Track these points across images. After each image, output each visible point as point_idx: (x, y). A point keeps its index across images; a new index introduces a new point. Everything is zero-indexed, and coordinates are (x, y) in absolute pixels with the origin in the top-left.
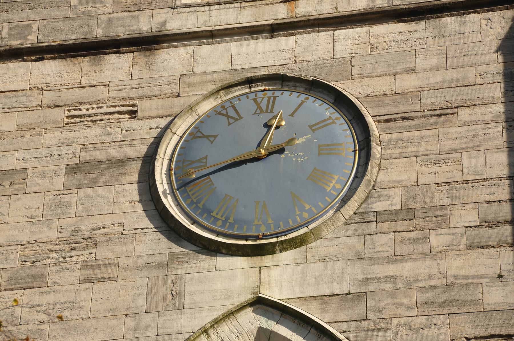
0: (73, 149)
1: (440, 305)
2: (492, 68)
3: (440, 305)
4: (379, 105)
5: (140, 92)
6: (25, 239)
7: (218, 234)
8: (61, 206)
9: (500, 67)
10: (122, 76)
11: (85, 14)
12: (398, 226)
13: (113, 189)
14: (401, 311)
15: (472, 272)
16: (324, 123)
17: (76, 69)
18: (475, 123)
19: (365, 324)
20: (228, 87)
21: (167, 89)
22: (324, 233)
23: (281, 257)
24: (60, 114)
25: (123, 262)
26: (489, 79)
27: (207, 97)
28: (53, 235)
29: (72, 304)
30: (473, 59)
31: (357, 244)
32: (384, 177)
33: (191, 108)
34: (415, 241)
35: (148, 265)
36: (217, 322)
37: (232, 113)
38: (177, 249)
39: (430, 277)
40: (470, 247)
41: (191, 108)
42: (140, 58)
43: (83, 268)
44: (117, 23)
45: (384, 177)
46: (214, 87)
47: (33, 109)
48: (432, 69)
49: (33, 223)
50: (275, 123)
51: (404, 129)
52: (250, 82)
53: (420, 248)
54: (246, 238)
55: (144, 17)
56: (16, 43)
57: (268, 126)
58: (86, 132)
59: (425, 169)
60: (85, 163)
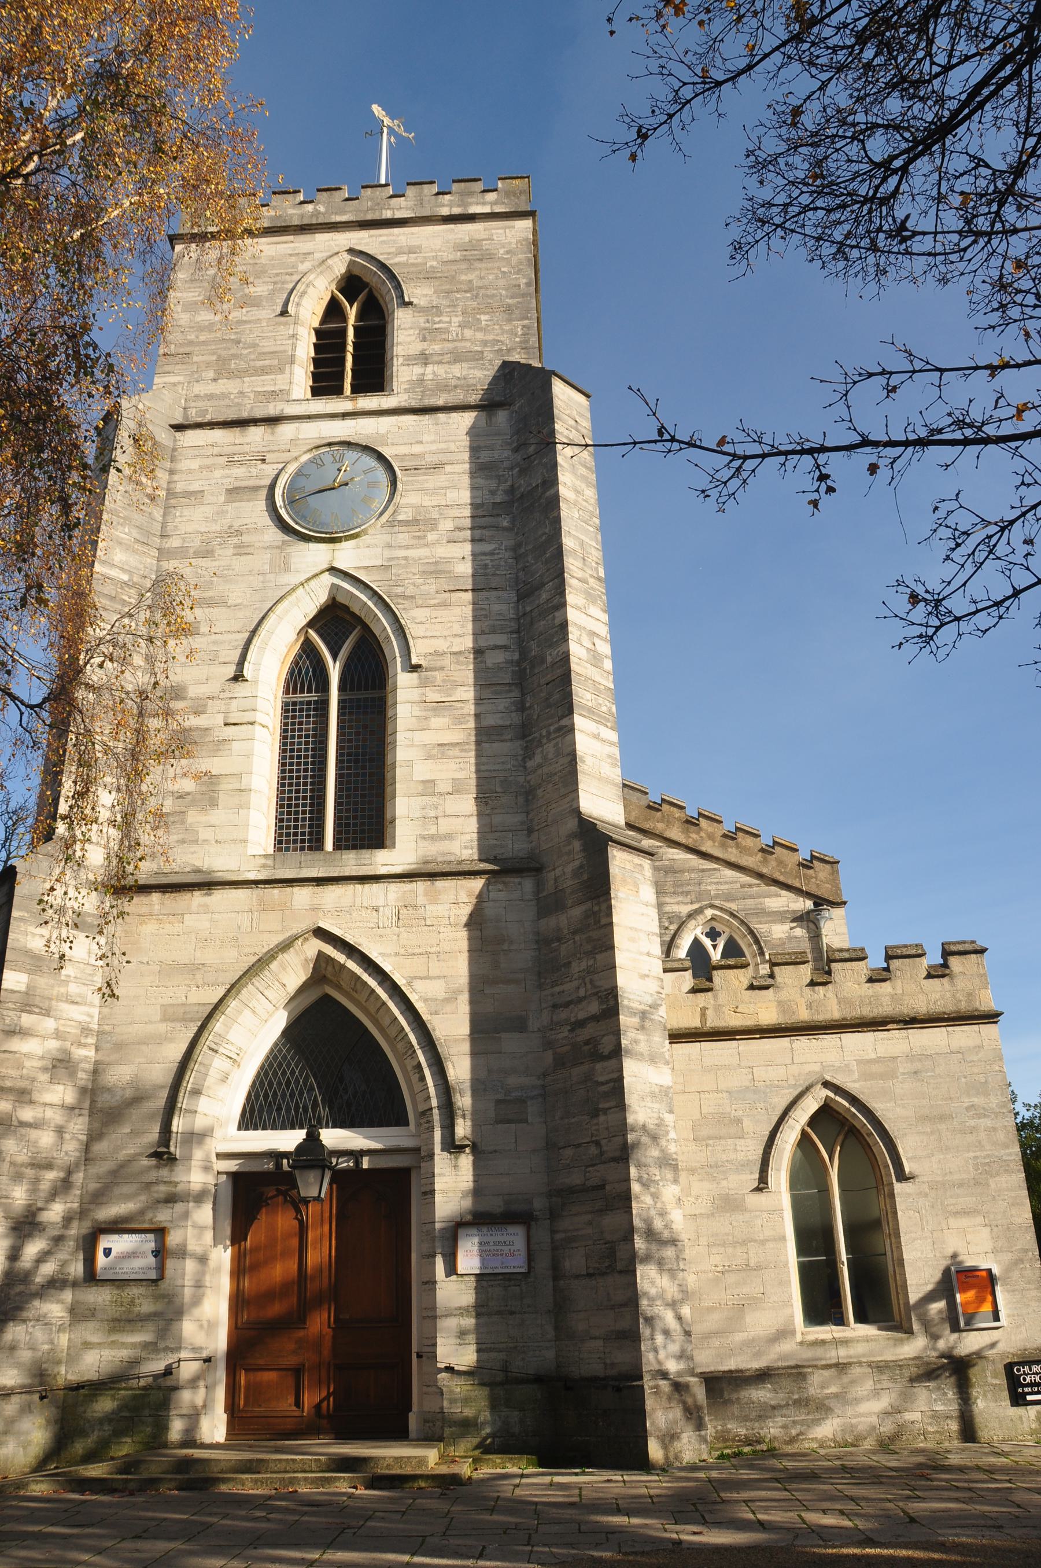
0: (229, 480)
1: (431, 573)
2: (463, 444)
3: (431, 573)
4: (402, 461)
5: (268, 449)
6: (203, 530)
7: (310, 530)
8: (223, 512)
9: (468, 443)
10: (258, 439)
11: (238, 404)
12: (410, 529)
13: (252, 503)
14: (410, 576)
15: (449, 555)
16: (371, 470)
17: (232, 435)
18: (454, 473)
19: (390, 583)
20: (318, 447)
21: (283, 447)
22: (370, 531)
23: (344, 544)
24: (223, 460)
25: (257, 545)
26: (462, 449)
27: (305, 453)
28: (218, 529)
29: (228, 567)
30: (454, 438)
31: (387, 538)
32: (403, 501)
33: (296, 458)
34: (419, 537)
35: (271, 547)
36: (309, 579)
37: (319, 462)
38: (287, 538)
39: (426, 557)
40: (449, 542)
41: (296, 458)
42: (268, 429)
43: (234, 547)
44: (255, 409)
45: (403, 501)
46: (310, 447)
47: (208, 456)
48: (431, 442)
49: (207, 522)
50: (344, 468)
51: (415, 475)
52: (330, 444)
53: (422, 541)
54: (326, 533)
55: (271, 406)
56: (199, 420)
57: (339, 470)
58: (238, 470)
59: (427, 498)
60: (236, 488)
